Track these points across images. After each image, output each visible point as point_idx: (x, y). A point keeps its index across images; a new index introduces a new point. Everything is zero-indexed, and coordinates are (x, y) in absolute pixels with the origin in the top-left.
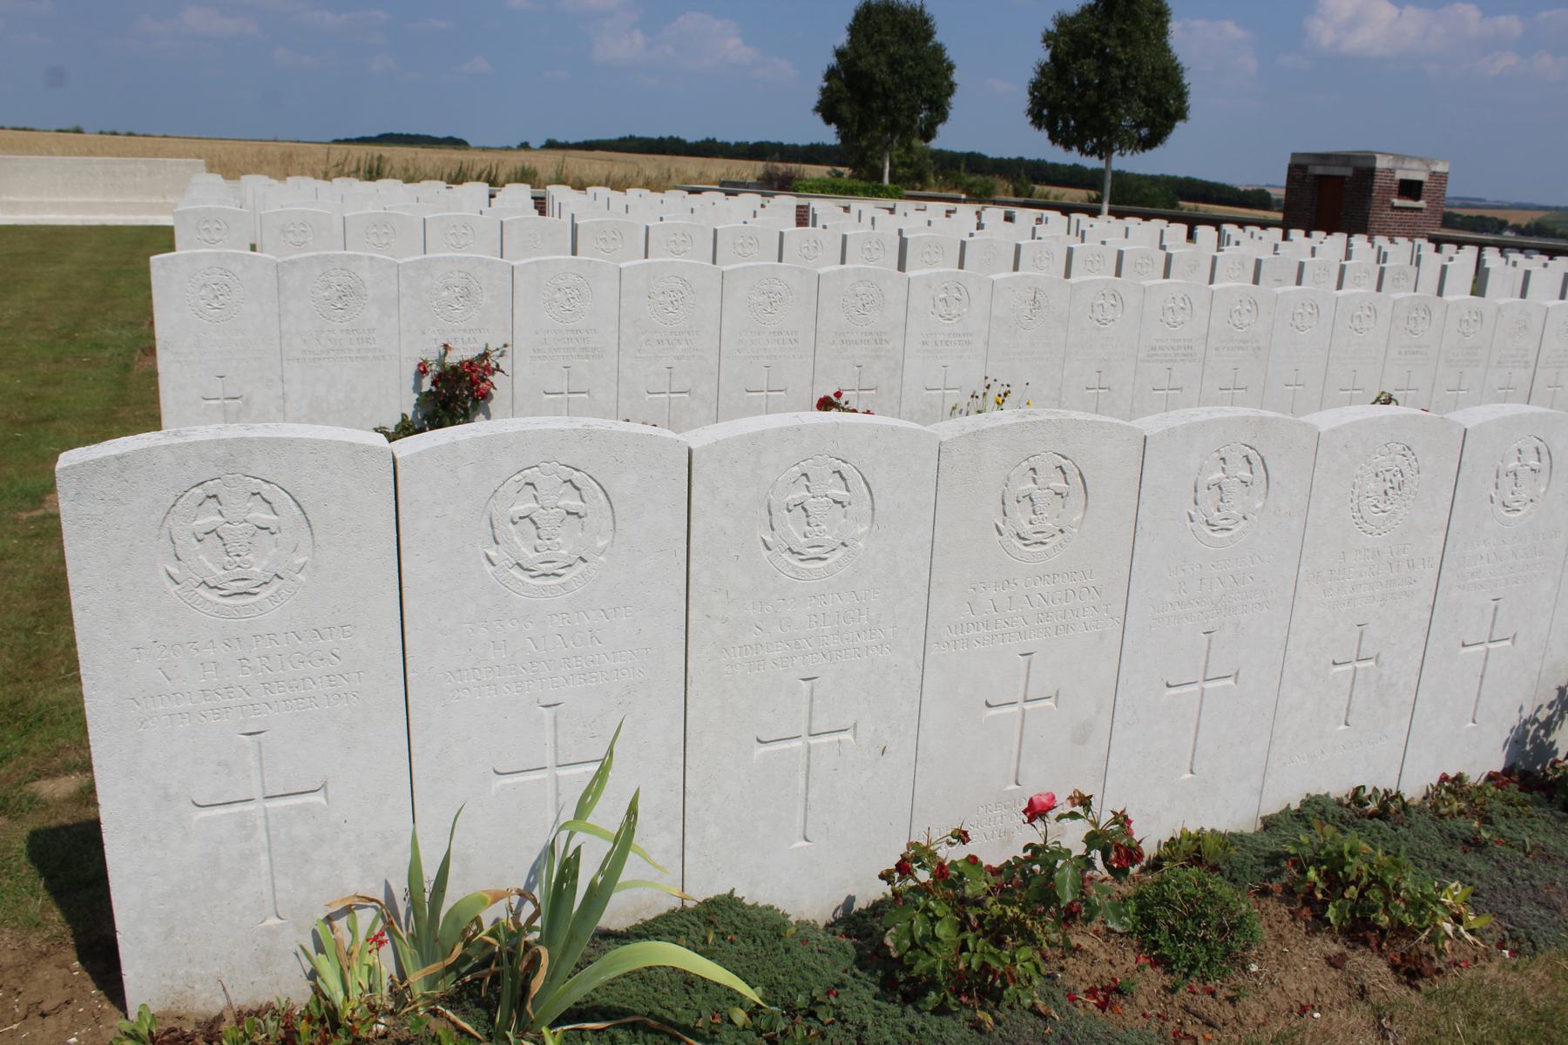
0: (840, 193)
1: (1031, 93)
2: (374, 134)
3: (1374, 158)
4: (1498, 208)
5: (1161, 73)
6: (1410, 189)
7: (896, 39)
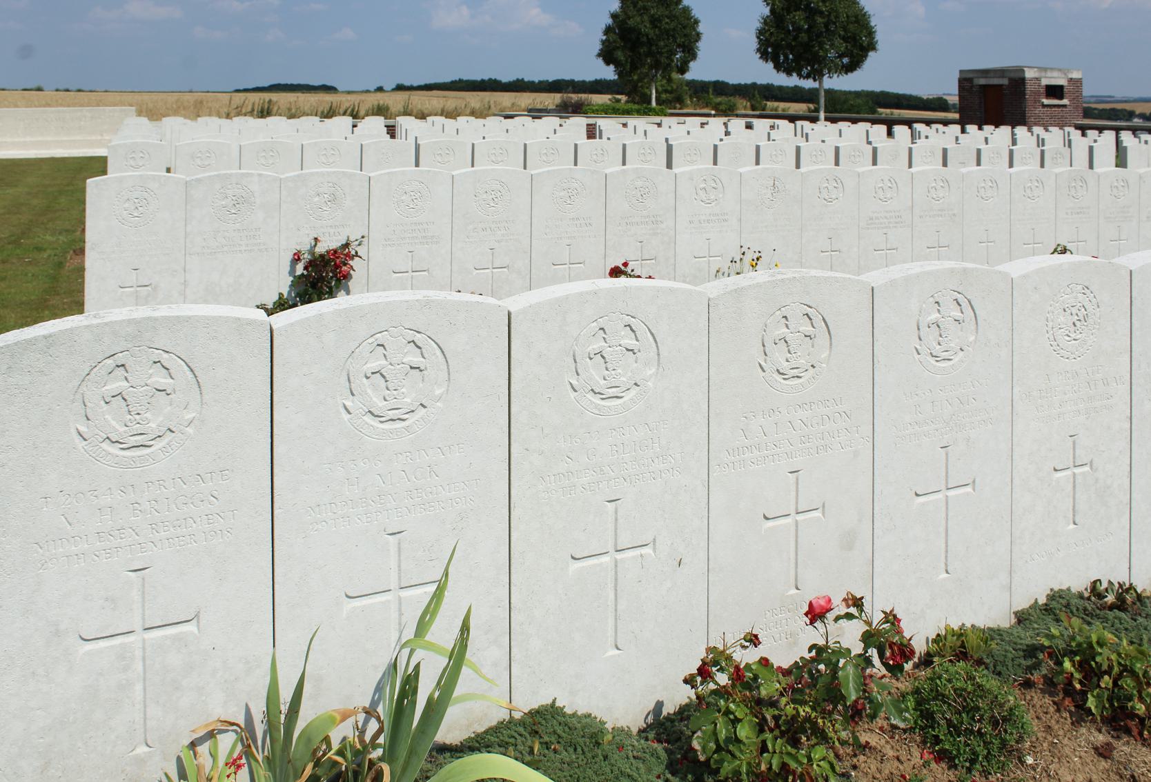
0: (619, 114)
1: (758, 37)
2: (266, 84)
3: (1024, 71)
4: (1126, 102)
5: (854, 19)
6: (1055, 91)
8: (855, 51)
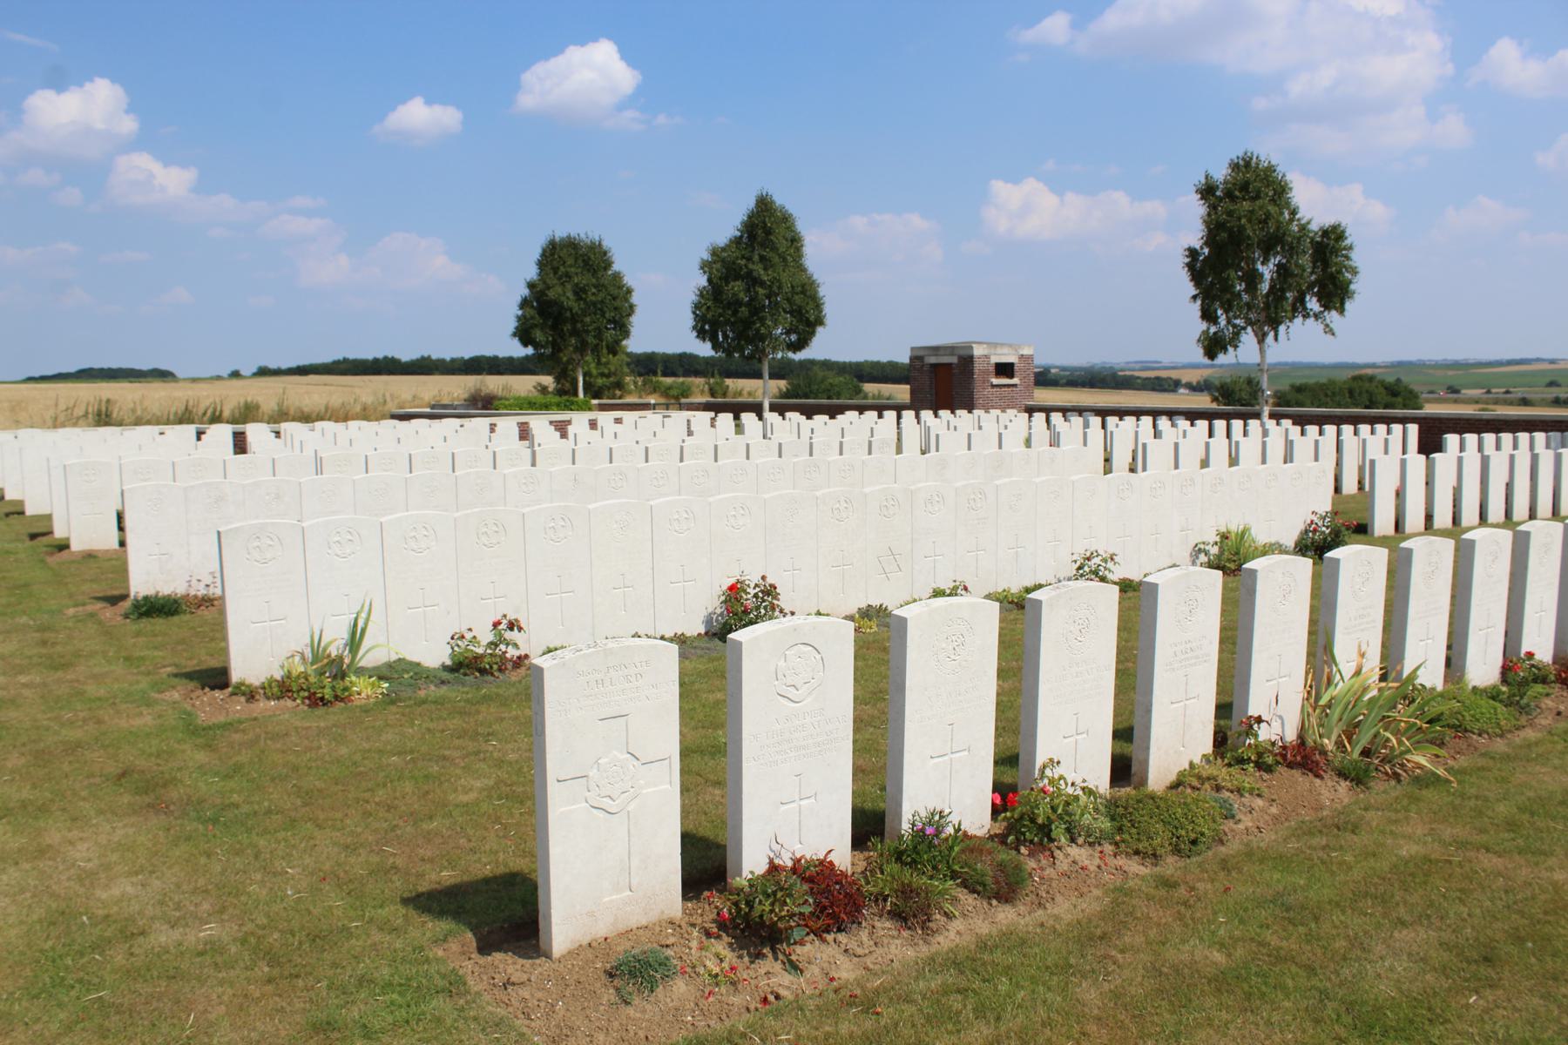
0: (536, 409)
1: (694, 313)
2: (73, 369)
5: (800, 289)
6: (1005, 370)
7: (580, 270)
8: (801, 327)
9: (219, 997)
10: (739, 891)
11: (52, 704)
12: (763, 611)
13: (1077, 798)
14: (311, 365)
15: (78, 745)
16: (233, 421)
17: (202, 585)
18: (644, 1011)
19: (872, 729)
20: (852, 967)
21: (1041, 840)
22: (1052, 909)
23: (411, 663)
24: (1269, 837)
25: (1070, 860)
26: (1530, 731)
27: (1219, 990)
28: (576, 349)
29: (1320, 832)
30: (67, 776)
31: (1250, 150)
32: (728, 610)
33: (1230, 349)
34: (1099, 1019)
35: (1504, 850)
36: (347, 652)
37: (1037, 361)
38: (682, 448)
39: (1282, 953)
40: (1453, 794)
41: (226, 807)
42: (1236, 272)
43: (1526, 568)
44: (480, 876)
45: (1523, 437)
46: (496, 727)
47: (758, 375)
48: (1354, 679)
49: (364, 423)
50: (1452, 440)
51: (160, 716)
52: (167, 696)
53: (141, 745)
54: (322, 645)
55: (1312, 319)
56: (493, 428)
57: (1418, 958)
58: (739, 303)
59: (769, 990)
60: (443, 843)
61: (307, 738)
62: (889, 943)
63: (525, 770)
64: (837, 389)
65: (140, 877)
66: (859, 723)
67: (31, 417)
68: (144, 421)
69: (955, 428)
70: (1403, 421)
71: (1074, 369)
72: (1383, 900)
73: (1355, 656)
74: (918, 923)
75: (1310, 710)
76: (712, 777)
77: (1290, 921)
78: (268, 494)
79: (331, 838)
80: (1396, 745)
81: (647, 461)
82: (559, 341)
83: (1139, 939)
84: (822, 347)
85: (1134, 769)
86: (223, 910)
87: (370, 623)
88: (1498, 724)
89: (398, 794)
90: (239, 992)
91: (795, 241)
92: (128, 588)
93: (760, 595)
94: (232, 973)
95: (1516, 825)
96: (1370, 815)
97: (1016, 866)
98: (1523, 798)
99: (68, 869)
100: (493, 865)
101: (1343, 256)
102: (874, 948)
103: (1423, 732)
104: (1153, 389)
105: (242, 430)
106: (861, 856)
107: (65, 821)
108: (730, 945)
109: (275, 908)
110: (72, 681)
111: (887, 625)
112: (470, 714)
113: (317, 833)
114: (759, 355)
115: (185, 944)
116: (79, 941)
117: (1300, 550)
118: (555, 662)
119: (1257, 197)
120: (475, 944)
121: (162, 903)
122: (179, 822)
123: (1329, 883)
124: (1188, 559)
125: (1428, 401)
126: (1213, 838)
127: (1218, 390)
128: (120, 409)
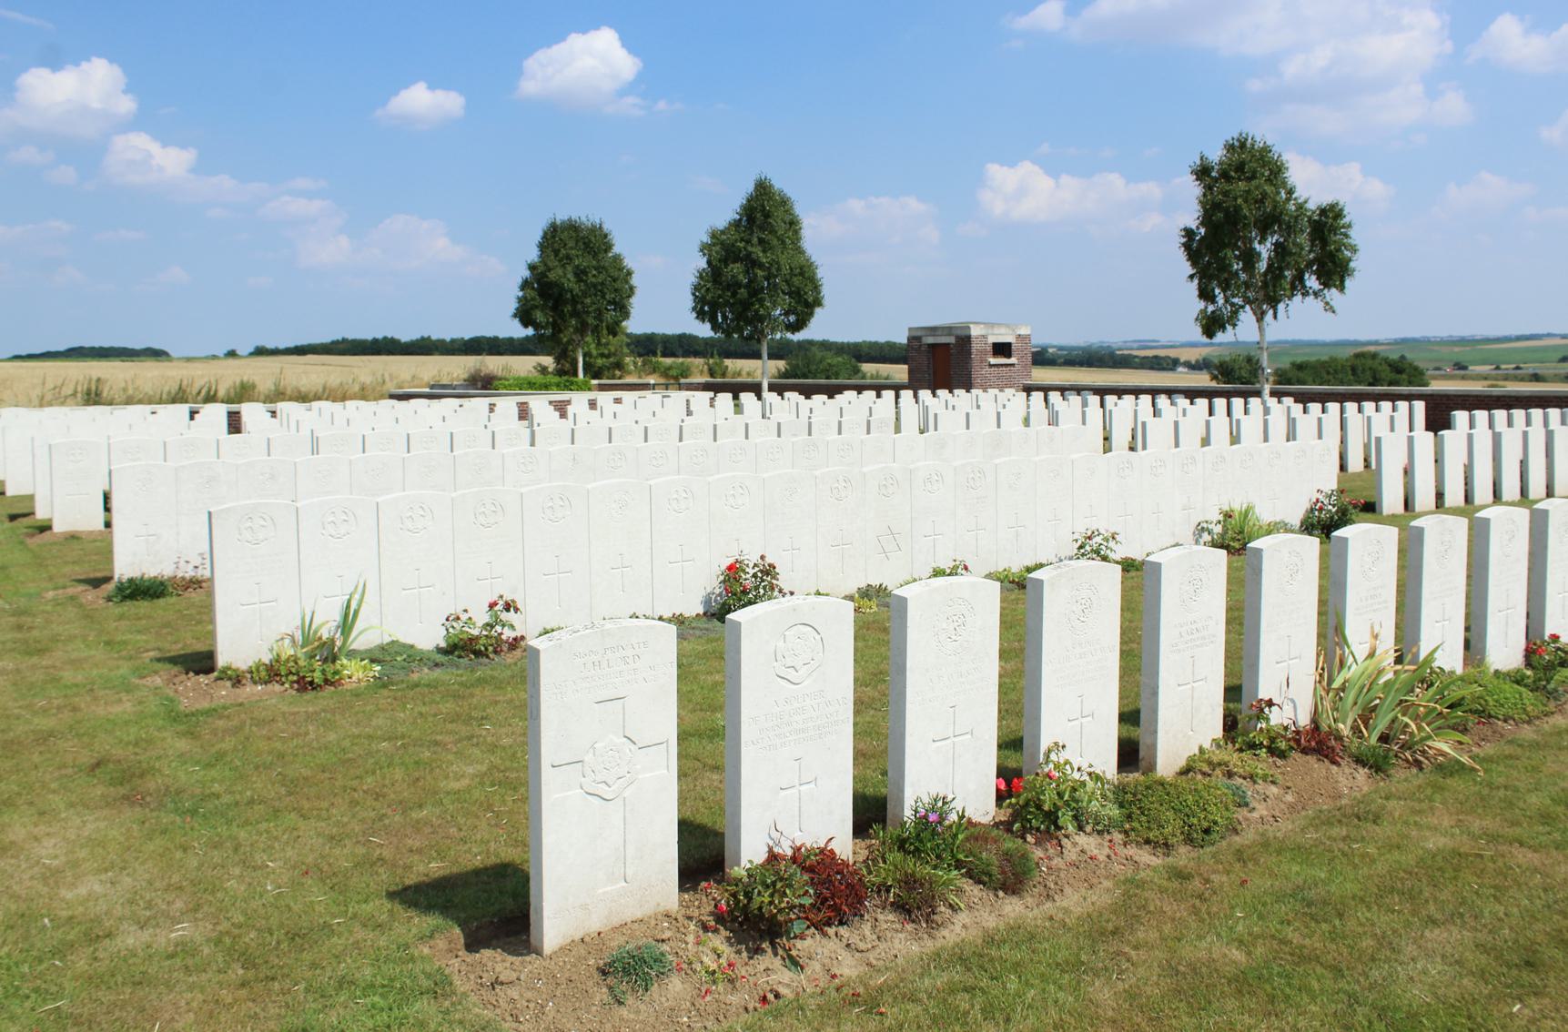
0: (536, 389)
1: (694, 294)
2: (62, 348)
3: (969, 328)
4: (1172, 347)
5: (798, 270)
6: (1002, 349)
8: (799, 308)
9: (187, 1004)
10: (738, 881)
11: (24, 691)
12: (762, 591)
13: (1083, 784)
14: (309, 345)
15: (51, 734)
16: (228, 401)
17: (190, 567)
18: (638, 1012)
19: (872, 712)
20: (855, 962)
21: (1048, 828)
22: (1061, 902)
23: (404, 645)
24: (1285, 826)
25: (1078, 849)
26: (1560, 718)
27: (1240, 992)
28: (577, 330)
29: (1340, 821)
30: (36, 767)
31: (1245, 131)
32: (726, 590)
33: (1229, 328)
34: (1114, 1022)
35: (1540, 844)
36: (339, 634)
37: (1034, 342)
38: (681, 427)
39: (1306, 952)
40: (1481, 784)
41: (205, 798)
42: (1233, 251)
43: (1545, 547)
44: (470, 867)
45: (1537, 413)
46: (490, 711)
47: (757, 356)
48: (1368, 662)
49: (362, 403)
50: (1460, 416)
51: (140, 703)
52: (148, 681)
53: (118, 733)
54: (314, 627)
55: (1312, 297)
56: (492, 408)
57: (1453, 960)
58: (739, 285)
59: (769, 988)
60: (433, 833)
61: (295, 724)
62: (892, 937)
63: (519, 755)
64: (835, 369)
65: (110, 874)
66: (860, 705)
67: (16, 396)
68: (135, 400)
69: (954, 408)
70: (1409, 398)
71: (1072, 349)
72: (1412, 896)
73: (1367, 637)
74: (922, 915)
75: (1323, 694)
76: (710, 761)
77: (1313, 918)
78: (262, 474)
79: (316, 828)
80: (1416, 731)
81: (646, 441)
82: (559, 321)
83: (1154, 935)
84: (820, 328)
85: (1142, 754)
86: (196, 909)
87: (363, 604)
88: (1525, 709)
89: (387, 782)
90: (210, 997)
91: (793, 224)
92: (112, 570)
93: (759, 574)
94: (204, 977)
95: (1551, 818)
96: (1392, 804)
97: (1023, 855)
98: (1556, 788)
99: (31, 868)
100: (483, 855)
101: (1341, 234)
102: (877, 942)
103: (1444, 717)
104: (1152, 368)
105: (237, 410)
106: (863, 844)
107: (32, 815)
108: (728, 939)
109: (254, 904)
110: (47, 668)
111: (887, 605)
112: (464, 697)
113: (301, 823)
114: (757, 336)
115: (155, 946)
116: (39, 945)
117: (1307, 529)
118: (551, 643)
119: (1253, 177)
120: (462, 941)
121: (131, 902)
122: (154, 814)
123: (1352, 877)
124: (1191, 538)
125: (1435, 378)
126: (1227, 827)
127: (1217, 368)
128: (111, 388)
